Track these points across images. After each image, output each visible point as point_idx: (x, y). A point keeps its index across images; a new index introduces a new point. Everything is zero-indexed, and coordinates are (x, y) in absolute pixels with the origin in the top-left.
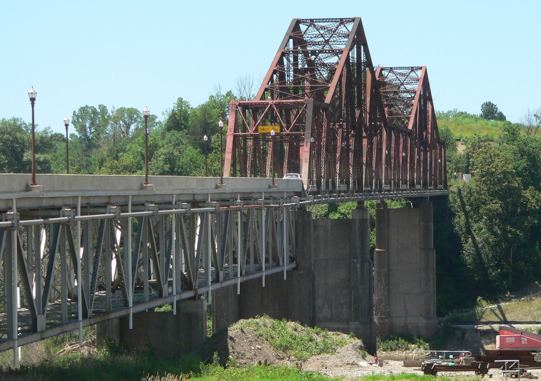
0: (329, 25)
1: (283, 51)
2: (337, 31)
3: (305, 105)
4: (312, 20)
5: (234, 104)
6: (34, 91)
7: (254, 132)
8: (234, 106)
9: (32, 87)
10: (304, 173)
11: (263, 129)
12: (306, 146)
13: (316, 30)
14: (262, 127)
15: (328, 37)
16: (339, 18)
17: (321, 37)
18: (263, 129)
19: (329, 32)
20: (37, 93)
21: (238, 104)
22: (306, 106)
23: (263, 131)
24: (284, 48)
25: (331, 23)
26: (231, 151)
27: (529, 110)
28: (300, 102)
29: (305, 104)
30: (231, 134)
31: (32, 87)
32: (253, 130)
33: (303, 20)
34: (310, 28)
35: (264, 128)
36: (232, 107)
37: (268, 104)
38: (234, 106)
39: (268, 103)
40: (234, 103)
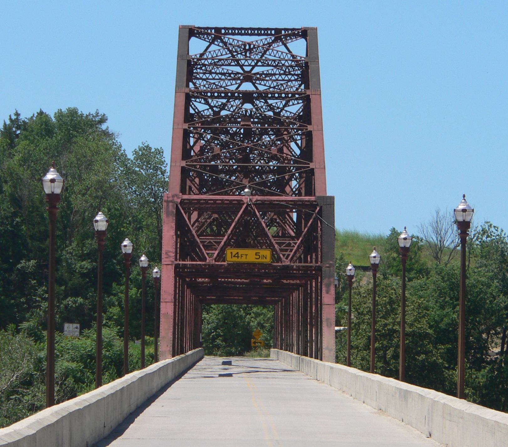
0: (259, 42)
1: (187, 90)
2: (270, 51)
3: (318, 208)
4: (218, 30)
5: (171, 202)
6: (468, 206)
7: (215, 261)
8: (171, 204)
9: (464, 196)
10: (327, 348)
11: (237, 255)
12: (327, 292)
13: (228, 52)
14: (235, 251)
15: (250, 65)
16: (214, 26)
17: (236, 65)
18: (237, 255)
19: (246, 55)
20: (473, 210)
21: (179, 201)
22: (321, 208)
23: (235, 259)
24: (188, 86)
25: (266, 37)
26: (170, 298)
27: (438, 213)
28: (306, 201)
29: (317, 205)
30: (170, 263)
31: (464, 196)
32: (215, 255)
33: (199, 28)
34: (213, 47)
35: (238, 253)
36: (168, 206)
37: (240, 203)
38: (171, 204)
39: (242, 200)
40: (171, 199)
